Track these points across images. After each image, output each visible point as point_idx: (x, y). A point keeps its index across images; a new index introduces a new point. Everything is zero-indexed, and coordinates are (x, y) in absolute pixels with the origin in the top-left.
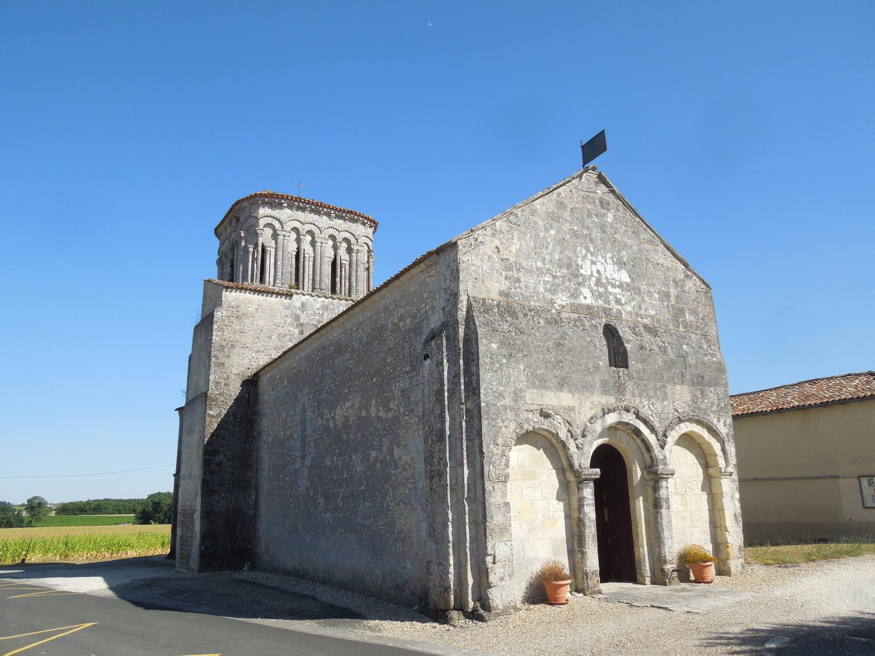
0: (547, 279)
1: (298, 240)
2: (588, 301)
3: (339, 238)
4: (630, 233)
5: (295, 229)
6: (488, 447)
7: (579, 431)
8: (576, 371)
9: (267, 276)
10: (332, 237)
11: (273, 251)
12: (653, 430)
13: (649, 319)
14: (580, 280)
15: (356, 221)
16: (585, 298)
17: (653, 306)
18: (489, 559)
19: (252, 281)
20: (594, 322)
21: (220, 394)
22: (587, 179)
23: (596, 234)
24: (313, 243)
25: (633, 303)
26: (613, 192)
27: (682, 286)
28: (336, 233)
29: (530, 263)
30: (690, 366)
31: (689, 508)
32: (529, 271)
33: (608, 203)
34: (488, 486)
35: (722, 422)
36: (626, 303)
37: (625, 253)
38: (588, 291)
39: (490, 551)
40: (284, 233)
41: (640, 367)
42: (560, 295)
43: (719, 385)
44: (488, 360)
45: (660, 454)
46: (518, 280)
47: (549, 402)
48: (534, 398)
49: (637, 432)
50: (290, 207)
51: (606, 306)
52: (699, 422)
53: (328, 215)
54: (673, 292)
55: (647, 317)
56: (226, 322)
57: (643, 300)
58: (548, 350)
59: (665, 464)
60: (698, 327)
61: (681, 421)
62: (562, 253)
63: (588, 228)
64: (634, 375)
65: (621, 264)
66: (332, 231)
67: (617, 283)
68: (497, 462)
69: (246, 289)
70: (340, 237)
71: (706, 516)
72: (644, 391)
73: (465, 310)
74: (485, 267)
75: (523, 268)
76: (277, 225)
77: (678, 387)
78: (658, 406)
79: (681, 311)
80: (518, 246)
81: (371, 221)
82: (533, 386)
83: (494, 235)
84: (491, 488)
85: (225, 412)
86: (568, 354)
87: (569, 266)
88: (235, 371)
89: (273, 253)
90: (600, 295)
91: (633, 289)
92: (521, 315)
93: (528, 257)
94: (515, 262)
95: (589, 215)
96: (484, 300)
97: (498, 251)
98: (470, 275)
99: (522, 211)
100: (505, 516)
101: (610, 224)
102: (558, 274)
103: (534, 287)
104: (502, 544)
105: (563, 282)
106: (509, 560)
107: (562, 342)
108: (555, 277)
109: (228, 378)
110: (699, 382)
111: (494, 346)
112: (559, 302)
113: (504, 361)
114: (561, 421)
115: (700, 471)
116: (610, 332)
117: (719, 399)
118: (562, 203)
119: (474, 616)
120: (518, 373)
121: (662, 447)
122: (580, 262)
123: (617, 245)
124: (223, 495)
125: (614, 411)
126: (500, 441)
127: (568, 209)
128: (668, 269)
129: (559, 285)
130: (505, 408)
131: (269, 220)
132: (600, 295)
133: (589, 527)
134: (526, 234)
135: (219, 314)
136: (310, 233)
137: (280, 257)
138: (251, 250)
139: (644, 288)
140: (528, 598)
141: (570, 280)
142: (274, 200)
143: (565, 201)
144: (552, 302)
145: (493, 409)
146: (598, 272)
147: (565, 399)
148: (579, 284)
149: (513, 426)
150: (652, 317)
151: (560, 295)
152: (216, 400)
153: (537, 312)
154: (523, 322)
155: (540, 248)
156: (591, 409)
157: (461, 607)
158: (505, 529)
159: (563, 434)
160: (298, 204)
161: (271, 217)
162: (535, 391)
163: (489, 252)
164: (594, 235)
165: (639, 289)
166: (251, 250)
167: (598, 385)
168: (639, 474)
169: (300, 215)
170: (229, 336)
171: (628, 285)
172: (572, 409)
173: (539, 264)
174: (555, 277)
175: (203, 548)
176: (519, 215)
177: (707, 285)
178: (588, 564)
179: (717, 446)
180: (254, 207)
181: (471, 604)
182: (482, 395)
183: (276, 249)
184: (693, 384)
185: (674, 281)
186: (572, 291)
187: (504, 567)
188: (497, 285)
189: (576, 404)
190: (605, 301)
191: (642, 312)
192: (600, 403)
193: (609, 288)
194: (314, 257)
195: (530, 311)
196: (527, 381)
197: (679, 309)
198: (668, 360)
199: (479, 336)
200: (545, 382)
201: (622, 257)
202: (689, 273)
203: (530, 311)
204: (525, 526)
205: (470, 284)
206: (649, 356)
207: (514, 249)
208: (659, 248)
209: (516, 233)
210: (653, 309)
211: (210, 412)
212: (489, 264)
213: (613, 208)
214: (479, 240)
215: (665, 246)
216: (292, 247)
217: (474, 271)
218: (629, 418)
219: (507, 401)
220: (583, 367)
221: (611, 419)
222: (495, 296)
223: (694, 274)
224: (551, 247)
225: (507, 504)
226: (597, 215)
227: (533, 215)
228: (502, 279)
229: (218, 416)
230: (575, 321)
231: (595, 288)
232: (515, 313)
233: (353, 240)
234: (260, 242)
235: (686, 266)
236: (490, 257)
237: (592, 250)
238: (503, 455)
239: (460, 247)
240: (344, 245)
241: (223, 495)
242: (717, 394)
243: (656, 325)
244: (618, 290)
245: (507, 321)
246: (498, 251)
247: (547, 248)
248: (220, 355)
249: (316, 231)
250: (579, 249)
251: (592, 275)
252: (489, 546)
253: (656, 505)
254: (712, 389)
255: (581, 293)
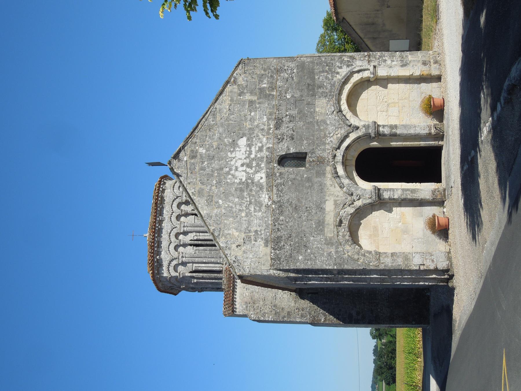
0: (253, 209)
1: (185, 245)
2: (264, 176)
3: (178, 212)
4: (211, 133)
5: (176, 248)
6: (360, 265)
7: (349, 198)
8: (312, 197)
9: (215, 269)
10: (178, 218)
11: (195, 265)
12: (347, 136)
13: (270, 122)
14: (250, 181)
15: (162, 198)
16: (262, 178)
17: (261, 118)
18: (422, 268)
19: (221, 279)
20: (278, 174)
21: (310, 314)
22: (178, 168)
23: (215, 165)
24: (185, 233)
25: (261, 136)
26: (183, 147)
27: (244, 88)
28: (175, 215)
29: (244, 222)
30: (302, 96)
31: (397, 101)
32: (249, 223)
33: (192, 151)
34: (382, 267)
35: (339, 70)
36: (261, 143)
37: (226, 140)
38: (256, 175)
39: (417, 268)
40: (180, 257)
41: (305, 142)
42: (262, 199)
43: (313, 69)
44: (309, 263)
45: (362, 131)
46: (256, 231)
47: (332, 220)
48: (330, 231)
49: (348, 148)
50: (159, 253)
51: (265, 160)
52: (340, 93)
53: (161, 222)
54: (248, 97)
55: (269, 125)
56: (258, 311)
57: (257, 126)
58: (300, 218)
59: (368, 126)
60: (272, 76)
61: (340, 111)
62: (233, 195)
63: (212, 171)
64: (311, 148)
65: (234, 144)
66: (174, 219)
67: (248, 149)
68: (368, 259)
69: (233, 298)
70: (177, 212)
71: (402, 86)
72: (321, 141)
73: (279, 272)
74: (251, 256)
75: (248, 227)
76: (174, 263)
77: (317, 110)
78: (331, 128)
79: (262, 90)
80: (234, 231)
81: (160, 184)
82: (322, 231)
83: (229, 249)
84: (383, 265)
85: (322, 311)
86: (302, 202)
87: (242, 190)
88: (293, 304)
89: (197, 265)
90: (258, 165)
91: (250, 134)
92: (279, 234)
93: (240, 223)
94: (245, 233)
95: (203, 169)
96: (272, 259)
97: (240, 246)
98: (257, 267)
99: (210, 226)
100: (398, 257)
101: (207, 151)
102: (248, 200)
103: (259, 220)
104: (414, 259)
105: (253, 196)
106: (422, 254)
107: (294, 206)
108: (251, 203)
109: (298, 309)
110: (312, 89)
111: (300, 258)
112: (266, 200)
113: (309, 251)
114: (343, 211)
115: (373, 87)
116: (283, 160)
117: (323, 72)
118: (199, 192)
119: (452, 277)
120: (315, 242)
121: (357, 128)
122: (237, 181)
123: (221, 146)
124: (379, 310)
125: (335, 168)
126: (356, 257)
127: (202, 187)
128: (232, 100)
129: (256, 200)
130: (337, 252)
131: (171, 269)
132: (258, 165)
133: (407, 195)
134: (225, 224)
135: (252, 316)
136: (177, 236)
137: (200, 260)
138: (195, 281)
139: (248, 125)
140: (445, 237)
141: (251, 190)
142: (156, 265)
143: (197, 189)
144: (267, 206)
145: (338, 261)
146: (242, 165)
147: (329, 206)
148: (253, 183)
149: (347, 247)
150: (269, 119)
151: (262, 199)
152: (314, 317)
153: (276, 220)
154: (283, 233)
155: (233, 213)
156: (335, 187)
157: (448, 280)
158: (406, 257)
159: (351, 210)
160: (155, 246)
161: (168, 268)
162: (326, 230)
163: (241, 253)
164: (217, 167)
165: (250, 129)
166: (195, 281)
167: (320, 179)
168: (375, 143)
169: (164, 244)
170: (268, 309)
171: (248, 140)
172: (336, 204)
173: (243, 214)
174: (251, 203)
175: (414, 323)
176: (213, 228)
177: (239, 64)
178: (428, 197)
179: (356, 78)
180: (162, 279)
181: (446, 276)
182: (330, 268)
183: (193, 263)
184: (314, 95)
185: (240, 95)
186: (258, 189)
187: (426, 259)
188: (261, 248)
189: (332, 199)
190: (262, 161)
191: (266, 128)
192: (331, 179)
193: (253, 156)
194: (196, 232)
195: (275, 225)
196: (320, 235)
197: (260, 93)
198: (299, 116)
199: (295, 268)
200: (320, 221)
201: (229, 142)
202: (232, 80)
203: (275, 225)
204: (405, 236)
205: (263, 268)
206: (297, 132)
207: (236, 234)
208: (218, 107)
209: (226, 232)
210: (261, 118)
211: (323, 320)
212: (249, 253)
213: (195, 147)
214: (234, 259)
215: (215, 102)
216: (190, 250)
217: (254, 264)
218: (340, 154)
219: (333, 250)
220: (309, 190)
221: (341, 170)
222: (268, 250)
223: (232, 75)
224: (231, 204)
225: (393, 254)
226: (203, 163)
227: (211, 217)
228: (257, 244)
229: (325, 315)
230: (278, 190)
231: (254, 169)
232: (278, 238)
233: (178, 200)
234: (190, 274)
235: (228, 82)
236: (244, 252)
237: (227, 169)
238: (364, 255)
239: (241, 273)
240: (183, 207)
241: (379, 310)
242: (320, 72)
243: (274, 117)
244: (253, 149)
245: (284, 245)
246: (240, 246)
247: (232, 207)
248: (282, 314)
249: (175, 231)
250: (228, 181)
251: (245, 171)
252: (415, 268)
253: (394, 136)
254: (317, 77)
255: (259, 181)
